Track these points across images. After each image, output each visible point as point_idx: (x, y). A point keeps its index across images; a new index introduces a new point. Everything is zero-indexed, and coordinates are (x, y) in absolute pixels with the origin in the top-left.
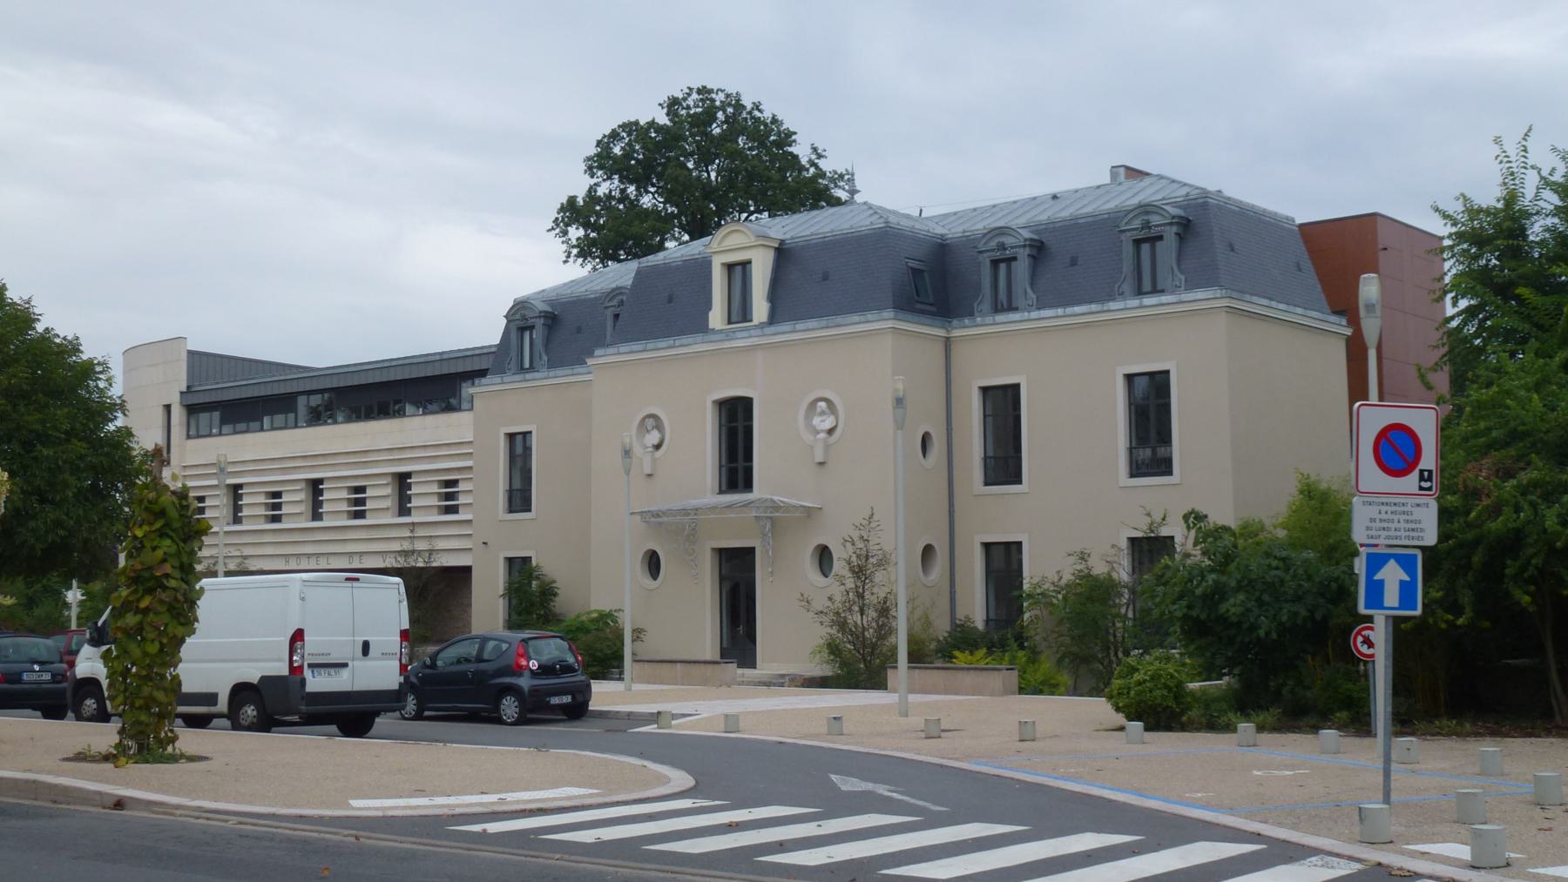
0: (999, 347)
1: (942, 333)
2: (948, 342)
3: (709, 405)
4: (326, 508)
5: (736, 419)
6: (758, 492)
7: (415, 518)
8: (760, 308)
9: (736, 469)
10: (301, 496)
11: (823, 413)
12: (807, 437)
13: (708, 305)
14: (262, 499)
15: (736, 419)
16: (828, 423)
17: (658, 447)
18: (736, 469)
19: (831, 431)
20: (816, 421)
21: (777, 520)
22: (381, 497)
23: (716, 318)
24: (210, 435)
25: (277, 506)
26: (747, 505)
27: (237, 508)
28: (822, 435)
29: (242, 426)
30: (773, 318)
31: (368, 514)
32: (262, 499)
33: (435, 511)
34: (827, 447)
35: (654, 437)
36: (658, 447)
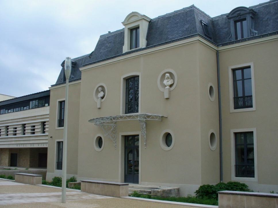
0: (236, 55)
1: (216, 48)
2: (217, 53)
3: (122, 80)
4: (26, 131)
5: (132, 84)
6: (140, 113)
7: (26, 135)
8: (143, 42)
9: (131, 104)
10: (40, 127)
11: (168, 78)
12: (161, 89)
13: (123, 44)
14: (30, 128)
15: (132, 84)
16: (170, 82)
17: (102, 98)
18: (131, 104)
19: (171, 86)
20: (165, 82)
21: (149, 122)
22: (19, 129)
23: (126, 48)
24: (18, 111)
25: (34, 130)
26: (137, 116)
27: (44, 129)
28: (168, 87)
29: (17, 109)
30: (149, 45)
31: (17, 134)
32: (30, 128)
33: (12, 135)
34: (170, 92)
35: (101, 94)
36: (102, 98)
